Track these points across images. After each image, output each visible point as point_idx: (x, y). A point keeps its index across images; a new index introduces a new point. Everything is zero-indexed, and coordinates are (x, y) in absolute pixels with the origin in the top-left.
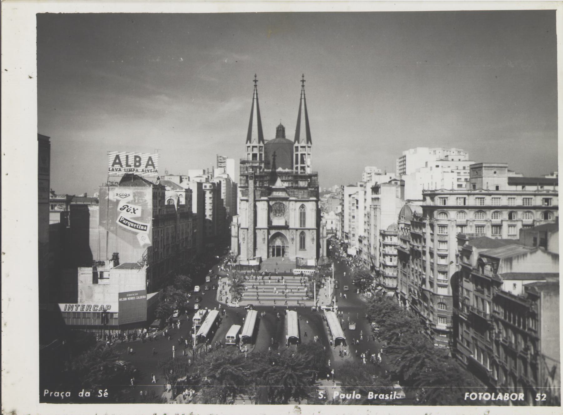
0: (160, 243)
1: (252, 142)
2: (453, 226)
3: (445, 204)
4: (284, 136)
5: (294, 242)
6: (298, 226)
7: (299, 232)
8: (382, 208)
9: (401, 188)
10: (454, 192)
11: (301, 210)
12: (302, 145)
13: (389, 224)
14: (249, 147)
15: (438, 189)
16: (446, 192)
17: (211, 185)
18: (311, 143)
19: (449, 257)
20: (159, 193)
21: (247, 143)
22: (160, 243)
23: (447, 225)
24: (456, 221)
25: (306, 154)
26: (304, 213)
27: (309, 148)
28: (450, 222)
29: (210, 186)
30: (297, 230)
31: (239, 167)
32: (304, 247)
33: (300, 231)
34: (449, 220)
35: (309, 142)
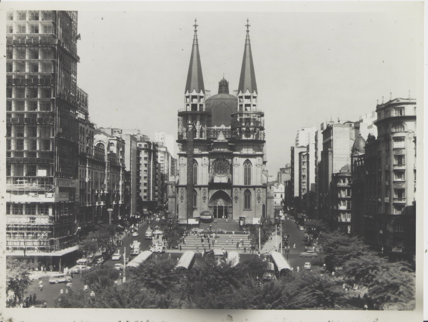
1: (191, 91)
3: (401, 114)
5: (238, 201)
6: (242, 183)
7: (243, 190)
8: (334, 151)
9: (355, 131)
11: (246, 166)
12: (246, 95)
14: (188, 97)
15: (392, 99)
16: (402, 101)
17: (146, 144)
18: (257, 93)
20: (87, 130)
23: (404, 137)
24: (414, 132)
25: (252, 105)
26: (249, 170)
27: (255, 99)
28: (407, 133)
30: (241, 187)
32: (249, 207)
33: (245, 189)
34: (406, 132)
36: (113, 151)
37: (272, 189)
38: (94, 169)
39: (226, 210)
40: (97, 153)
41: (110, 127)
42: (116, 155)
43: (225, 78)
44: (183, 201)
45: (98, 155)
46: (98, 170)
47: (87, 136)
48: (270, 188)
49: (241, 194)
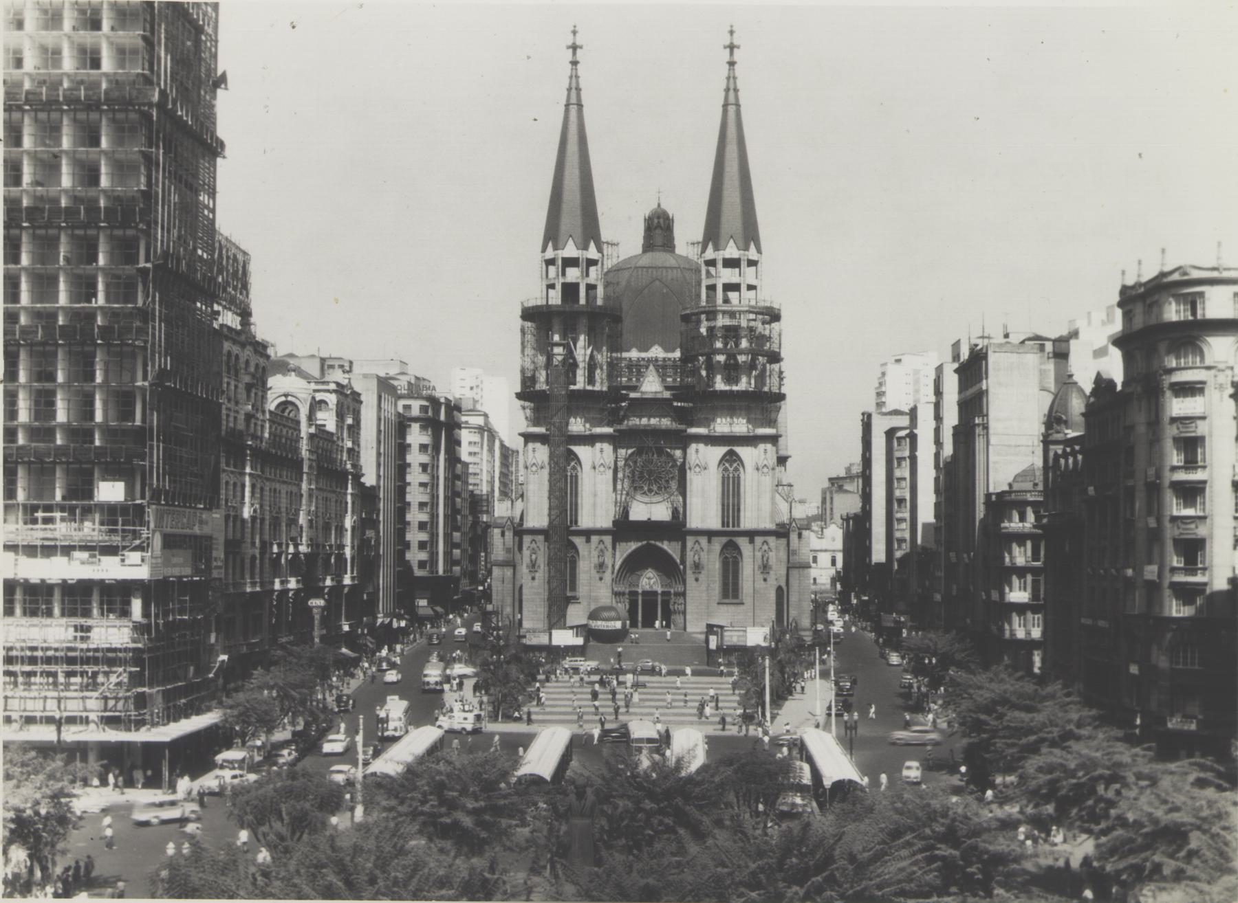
0: (258, 561)
1: (560, 245)
2: (1221, 385)
3: (1194, 313)
4: (669, 245)
5: (702, 577)
6: (714, 523)
7: (718, 543)
9: (1056, 364)
10: (1226, 274)
11: (726, 470)
12: (728, 256)
13: (1019, 470)
14: (550, 262)
16: (1196, 274)
17: (425, 403)
18: (759, 251)
19: (1211, 487)
20: (247, 362)
21: (544, 250)
22: (258, 561)
24: (1232, 368)
25: (744, 288)
26: (737, 482)
28: (1213, 372)
29: (424, 409)
30: (710, 534)
31: (519, 328)
32: (736, 595)
33: (724, 540)
35: (752, 246)
36: (324, 426)
37: (803, 541)
38: (268, 479)
39: (666, 604)
40: (278, 431)
41: (316, 354)
42: (335, 439)
43: (663, 206)
44: (537, 575)
45: (281, 437)
46: (279, 481)
47: (247, 379)
48: (800, 536)
49: (711, 556)
